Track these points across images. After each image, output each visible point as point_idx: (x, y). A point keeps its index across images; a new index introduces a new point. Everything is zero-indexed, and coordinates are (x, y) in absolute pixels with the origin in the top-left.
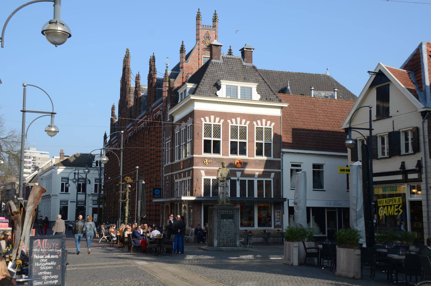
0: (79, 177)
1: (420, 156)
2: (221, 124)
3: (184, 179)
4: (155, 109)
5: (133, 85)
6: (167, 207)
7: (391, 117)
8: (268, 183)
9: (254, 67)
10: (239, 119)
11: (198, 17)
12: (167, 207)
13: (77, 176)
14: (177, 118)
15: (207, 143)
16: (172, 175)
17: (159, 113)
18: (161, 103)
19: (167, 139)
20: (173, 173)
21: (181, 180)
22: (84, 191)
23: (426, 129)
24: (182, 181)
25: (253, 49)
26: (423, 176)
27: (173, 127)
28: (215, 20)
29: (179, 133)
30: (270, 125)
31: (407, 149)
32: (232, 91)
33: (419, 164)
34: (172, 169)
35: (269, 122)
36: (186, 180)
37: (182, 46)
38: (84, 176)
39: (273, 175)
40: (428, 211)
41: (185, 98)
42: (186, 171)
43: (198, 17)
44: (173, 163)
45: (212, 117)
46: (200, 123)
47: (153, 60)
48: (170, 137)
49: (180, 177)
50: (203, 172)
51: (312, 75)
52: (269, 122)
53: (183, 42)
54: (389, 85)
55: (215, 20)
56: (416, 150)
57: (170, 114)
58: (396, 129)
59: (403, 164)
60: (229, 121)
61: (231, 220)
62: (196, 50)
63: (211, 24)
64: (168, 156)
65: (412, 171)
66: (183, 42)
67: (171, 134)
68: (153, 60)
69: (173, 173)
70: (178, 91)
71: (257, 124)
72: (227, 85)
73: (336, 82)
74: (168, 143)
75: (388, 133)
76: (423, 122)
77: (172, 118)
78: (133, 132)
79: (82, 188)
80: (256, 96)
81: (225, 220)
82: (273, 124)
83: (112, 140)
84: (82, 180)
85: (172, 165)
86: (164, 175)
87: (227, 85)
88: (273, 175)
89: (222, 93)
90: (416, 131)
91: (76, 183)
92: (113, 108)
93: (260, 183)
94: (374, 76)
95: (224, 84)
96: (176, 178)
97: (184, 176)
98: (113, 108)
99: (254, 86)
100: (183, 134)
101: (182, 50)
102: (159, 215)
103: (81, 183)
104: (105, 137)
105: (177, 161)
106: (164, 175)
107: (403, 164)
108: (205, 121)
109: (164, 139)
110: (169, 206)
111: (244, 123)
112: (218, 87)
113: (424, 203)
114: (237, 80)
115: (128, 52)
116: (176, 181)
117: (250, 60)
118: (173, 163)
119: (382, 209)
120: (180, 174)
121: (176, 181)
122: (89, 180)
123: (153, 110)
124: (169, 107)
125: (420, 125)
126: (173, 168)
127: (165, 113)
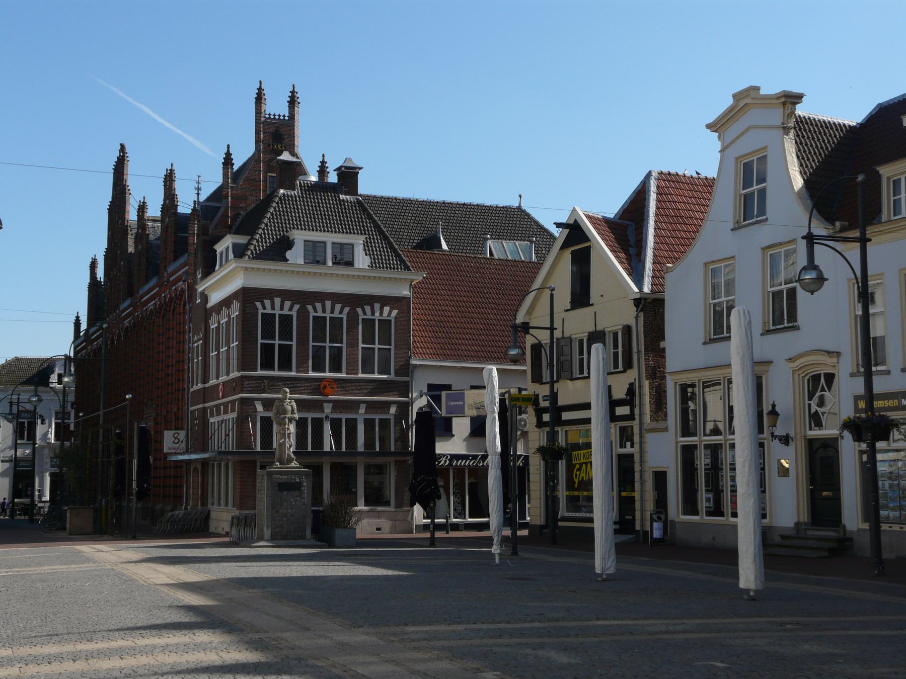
0: (21, 408)
1: (631, 376)
2: (294, 313)
3: (226, 417)
4: (174, 277)
5: (132, 215)
8: (384, 423)
11: (260, 98)
12: (196, 469)
13: (15, 408)
14: (215, 298)
16: (204, 409)
18: (185, 266)
19: (196, 338)
20: (207, 405)
21: (220, 418)
22: (32, 436)
23: (641, 329)
24: (222, 421)
26: (637, 411)
27: (207, 314)
29: (218, 328)
30: (341, 313)
32: (314, 254)
33: (631, 391)
34: (204, 396)
35: (287, 304)
38: (29, 407)
39: (393, 410)
40: (641, 472)
42: (229, 402)
43: (260, 98)
44: (207, 385)
47: (169, 179)
48: (201, 335)
49: (219, 414)
51: (490, 208)
53: (228, 146)
54: (590, 247)
55: (293, 102)
56: (628, 365)
57: (200, 290)
58: (599, 328)
60: (359, 310)
61: (296, 493)
64: (198, 371)
65: (621, 403)
66: (228, 146)
67: (203, 329)
68: (169, 179)
70: (216, 247)
71: (315, 311)
74: (198, 346)
76: (637, 317)
77: (205, 298)
78: (133, 318)
80: (362, 261)
81: (285, 493)
82: (395, 312)
83: (91, 331)
84: (26, 415)
85: (204, 388)
86: (191, 409)
88: (393, 410)
89: (296, 255)
90: (627, 330)
91: (15, 423)
95: (300, 237)
96: (212, 416)
97: (226, 412)
98: (93, 265)
99: (358, 241)
100: (223, 331)
102: (181, 487)
103: (26, 421)
104: (77, 323)
105: (213, 382)
106: (191, 409)
109: (189, 338)
110: (200, 468)
111: (342, 313)
112: (288, 244)
113: (637, 458)
114: (327, 229)
115: (123, 148)
116: (212, 420)
118: (207, 385)
119: (578, 470)
120: (218, 407)
122: (41, 416)
123: (171, 279)
124: (199, 276)
125: (632, 322)
127: (192, 289)
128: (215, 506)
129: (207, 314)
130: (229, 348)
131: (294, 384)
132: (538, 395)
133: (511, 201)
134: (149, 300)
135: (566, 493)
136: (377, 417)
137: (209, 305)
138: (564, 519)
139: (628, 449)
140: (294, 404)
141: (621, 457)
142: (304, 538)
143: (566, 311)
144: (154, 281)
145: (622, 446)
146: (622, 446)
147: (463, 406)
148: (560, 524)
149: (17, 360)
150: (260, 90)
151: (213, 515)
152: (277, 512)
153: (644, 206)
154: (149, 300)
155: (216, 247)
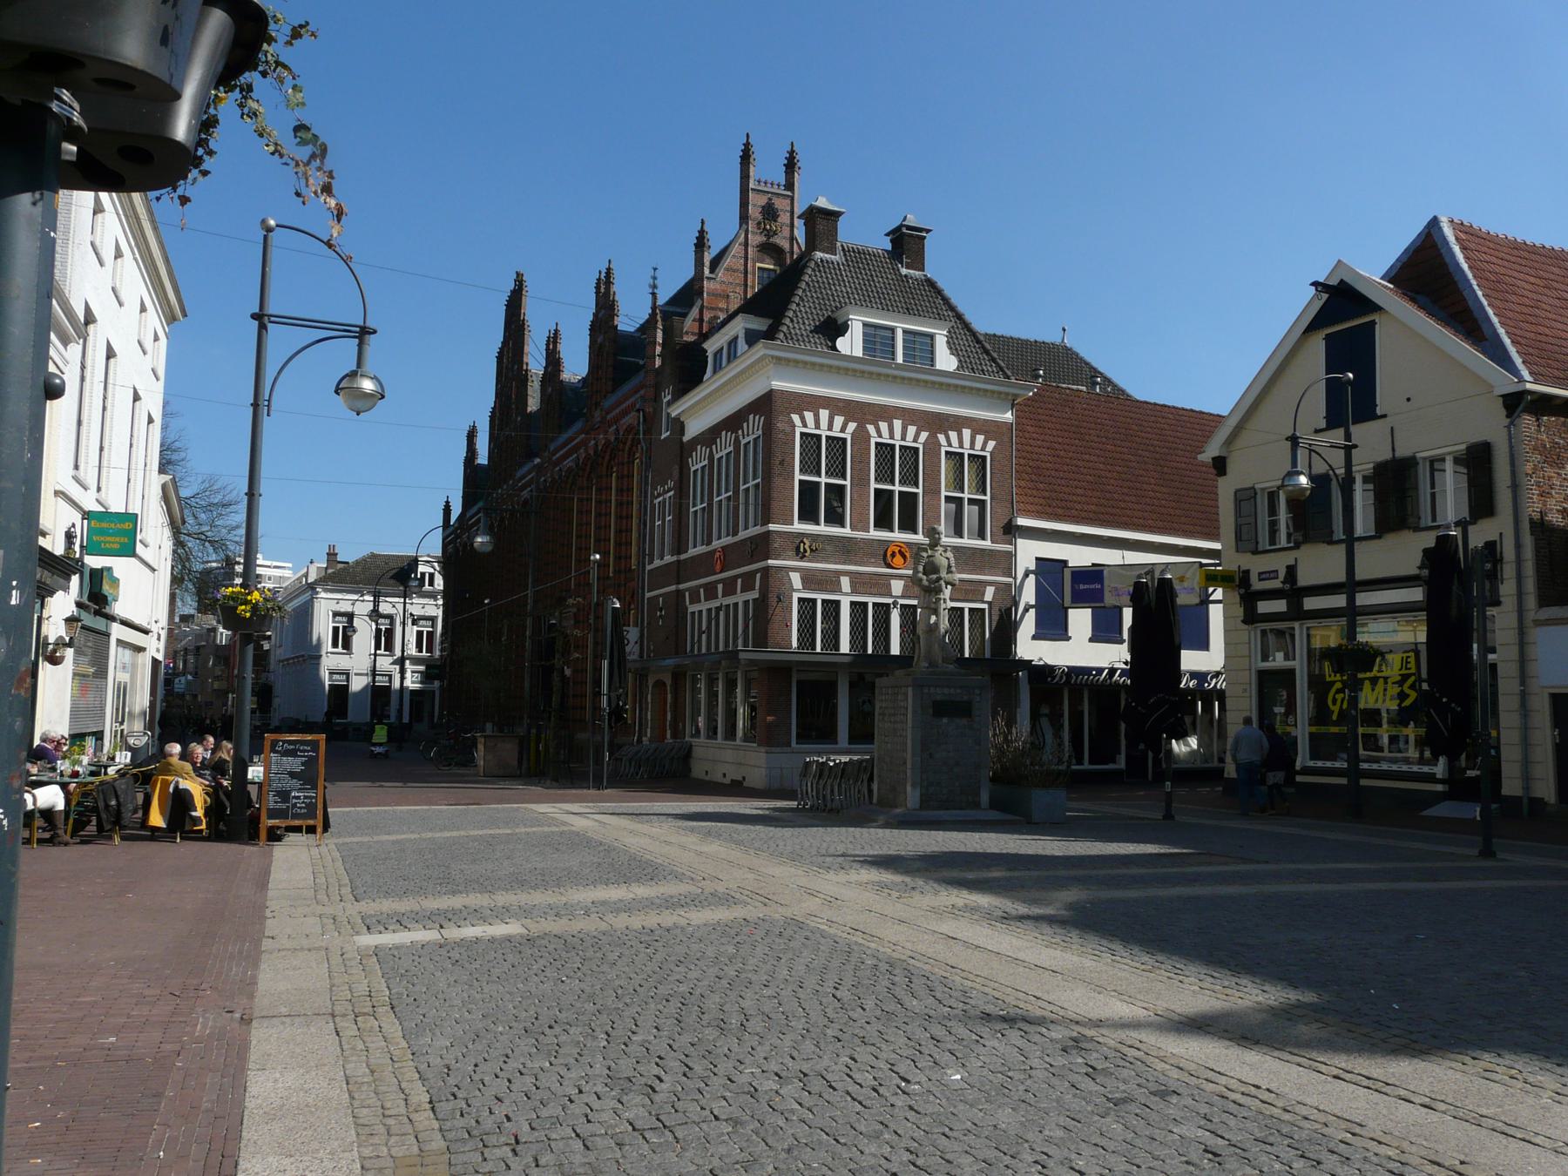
3: (730, 600)
5: (535, 363)
6: (660, 685)
7: (1384, 416)
8: (832, 608)
9: (931, 283)
10: (898, 424)
11: (746, 157)
14: (694, 428)
15: (809, 490)
16: (679, 594)
17: (629, 420)
20: (682, 586)
21: (714, 604)
24: (718, 609)
25: (928, 231)
27: (684, 451)
28: (791, 165)
30: (843, 430)
31: (1273, 541)
32: (877, 340)
36: (736, 604)
37: (702, 232)
39: (989, 593)
41: (729, 361)
43: (746, 157)
44: (683, 557)
45: (824, 414)
46: (788, 429)
48: (671, 484)
50: (796, 578)
52: (912, 430)
55: (791, 165)
58: (1403, 452)
59: (1291, 571)
60: (871, 428)
61: (964, 721)
62: (737, 249)
63: (781, 178)
67: (676, 473)
69: (682, 586)
70: (705, 346)
71: (879, 433)
72: (865, 325)
73: (1087, 364)
75: (1463, 447)
79: (385, 639)
81: (945, 720)
82: (991, 444)
86: (648, 595)
87: (865, 325)
89: (851, 344)
92: (471, 435)
93: (858, 609)
94: (1325, 296)
95: (857, 323)
98: (471, 435)
101: (701, 244)
104: (447, 510)
106: (648, 595)
107: (1291, 571)
108: (803, 424)
110: (669, 682)
111: (915, 438)
116: (692, 608)
117: (919, 263)
118: (683, 557)
121: (692, 608)
126: (679, 572)
127: (651, 421)
128: (702, 739)
129: (684, 451)
130: (710, 505)
131: (846, 549)
132: (1247, 572)
133: (1051, 336)
134: (565, 457)
135: (1379, 731)
136: (820, 597)
137: (686, 439)
138: (1306, 771)
139: (1278, 661)
140: (950, 554)
141: (1263, 675)
142: (977, 805)
143: (1317, 431)
144: (578, 425)
145: (1265, 658)
146: (1265, 658)
147: (1102, 590)
148: (1299, 778)
149: (373, 556)
150: (747, 145)
151: (698, 752)
152: (931, 755)
153: (1444, 265)
154: (565, 457)
155: (705, 346)
